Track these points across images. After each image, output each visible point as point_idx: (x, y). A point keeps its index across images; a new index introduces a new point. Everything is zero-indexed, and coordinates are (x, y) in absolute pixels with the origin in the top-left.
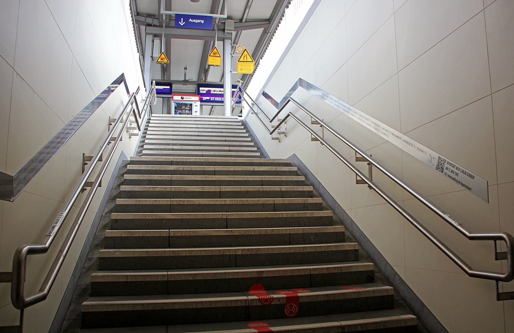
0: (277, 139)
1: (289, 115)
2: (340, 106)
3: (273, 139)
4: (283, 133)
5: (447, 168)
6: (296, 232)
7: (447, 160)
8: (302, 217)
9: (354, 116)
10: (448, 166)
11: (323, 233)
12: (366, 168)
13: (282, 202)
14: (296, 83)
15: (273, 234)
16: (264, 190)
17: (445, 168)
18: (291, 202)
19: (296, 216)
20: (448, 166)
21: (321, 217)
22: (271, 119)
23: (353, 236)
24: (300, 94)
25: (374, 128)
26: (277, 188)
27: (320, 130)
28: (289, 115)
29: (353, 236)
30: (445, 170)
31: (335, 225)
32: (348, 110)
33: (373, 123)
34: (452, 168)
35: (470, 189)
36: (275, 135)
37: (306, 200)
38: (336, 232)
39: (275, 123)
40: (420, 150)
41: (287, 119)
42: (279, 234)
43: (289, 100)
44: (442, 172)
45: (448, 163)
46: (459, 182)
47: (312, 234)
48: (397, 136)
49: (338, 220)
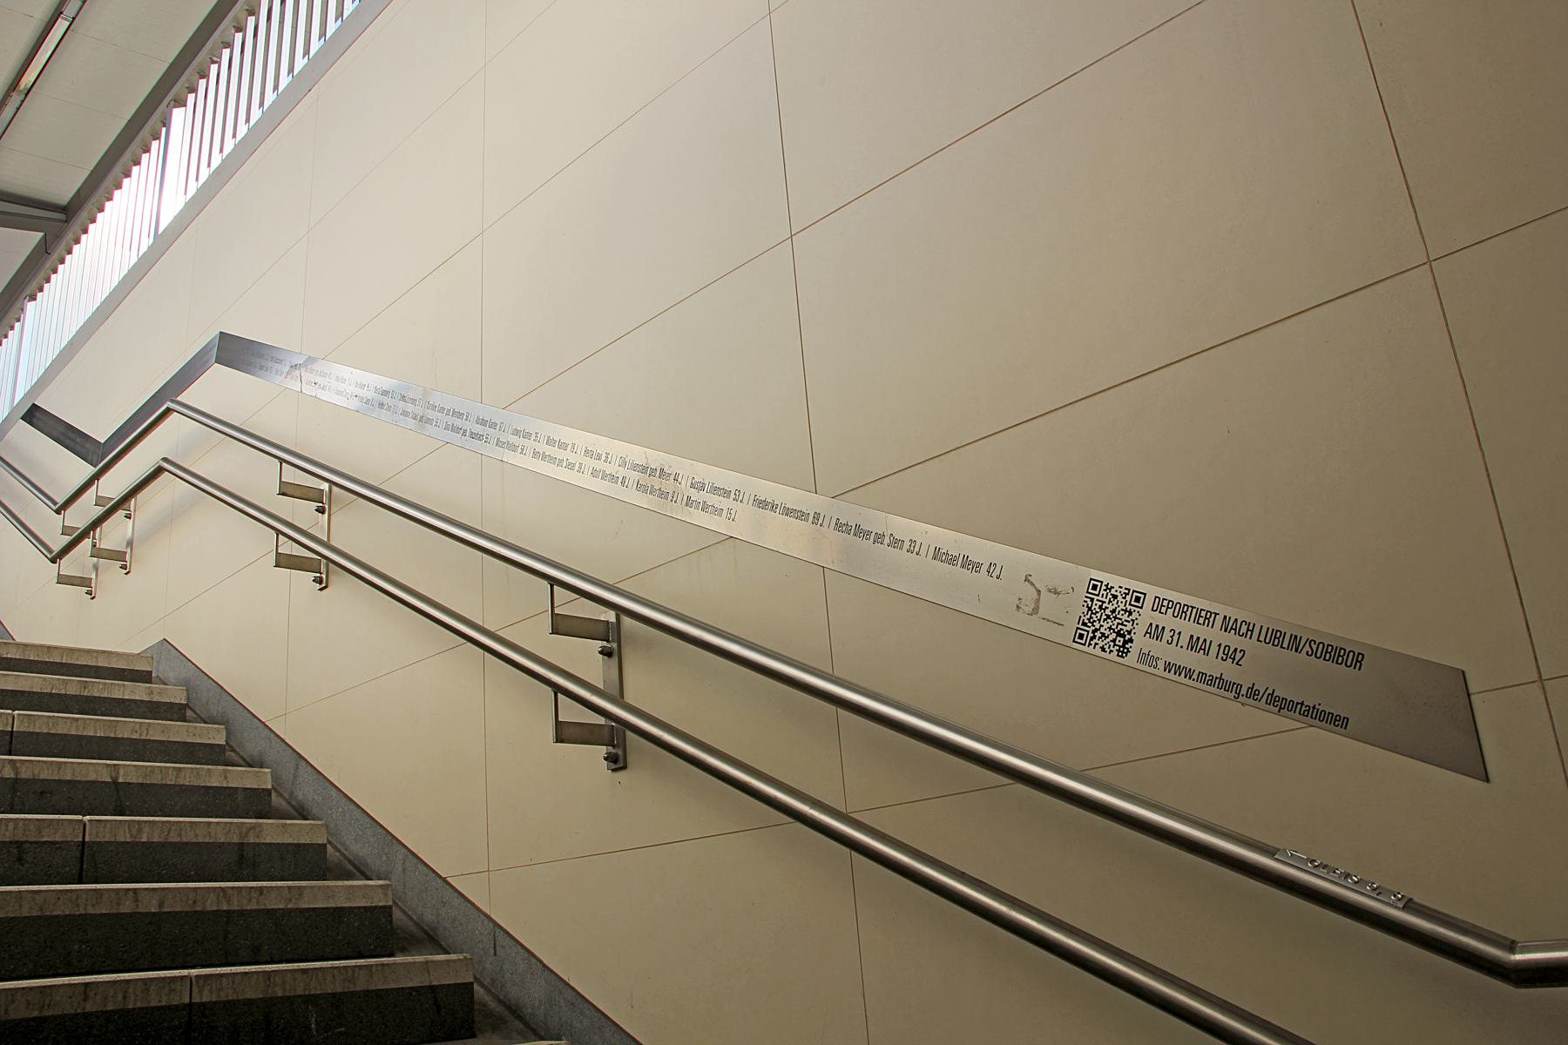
0: (84, 582)
1: (159, 471)
2: (431, 414)
3: (63, 580)
4: (118, 556)
5: (1155, 632)
6: (227, 994)
7: (1152, 591)
8: (242, 913)
9: (513, 448)
10: (1167, 620)
11: (367, 993)
12: (605, 669)
13: (124, 836)
14: (204, 351)
15: (86, 1015)
16: (25, 774)
17: (1140, 630)
18: (174, 838)
19: (211, 906)
20: (1167, 620)
21: (338, 912)
22: (61, 501)
23: (509, 1008)
24: (219, 389)
25: (639, 486)
26: (95, 769)
27: (314, 522)
28: (159, 471)
29: (509, 1008)
30: (1140, 642)
31: (404, 951)
32: (478, 429)
33: (635, 467)
34: (1188, 628)
35: (1338, 722)
36: (68, 566)
37: (254, 827)
38: (433, 988)
39: (85, 510)
40: (952, 560)
41: (140, 496)
42: (124, 1013)
43: (168, 411)
44: (1123, 651)
45: (1160, 605)
46: (1253, 693)
47: (310, 1000)
48: (788, 512)
49: (413, 928)
